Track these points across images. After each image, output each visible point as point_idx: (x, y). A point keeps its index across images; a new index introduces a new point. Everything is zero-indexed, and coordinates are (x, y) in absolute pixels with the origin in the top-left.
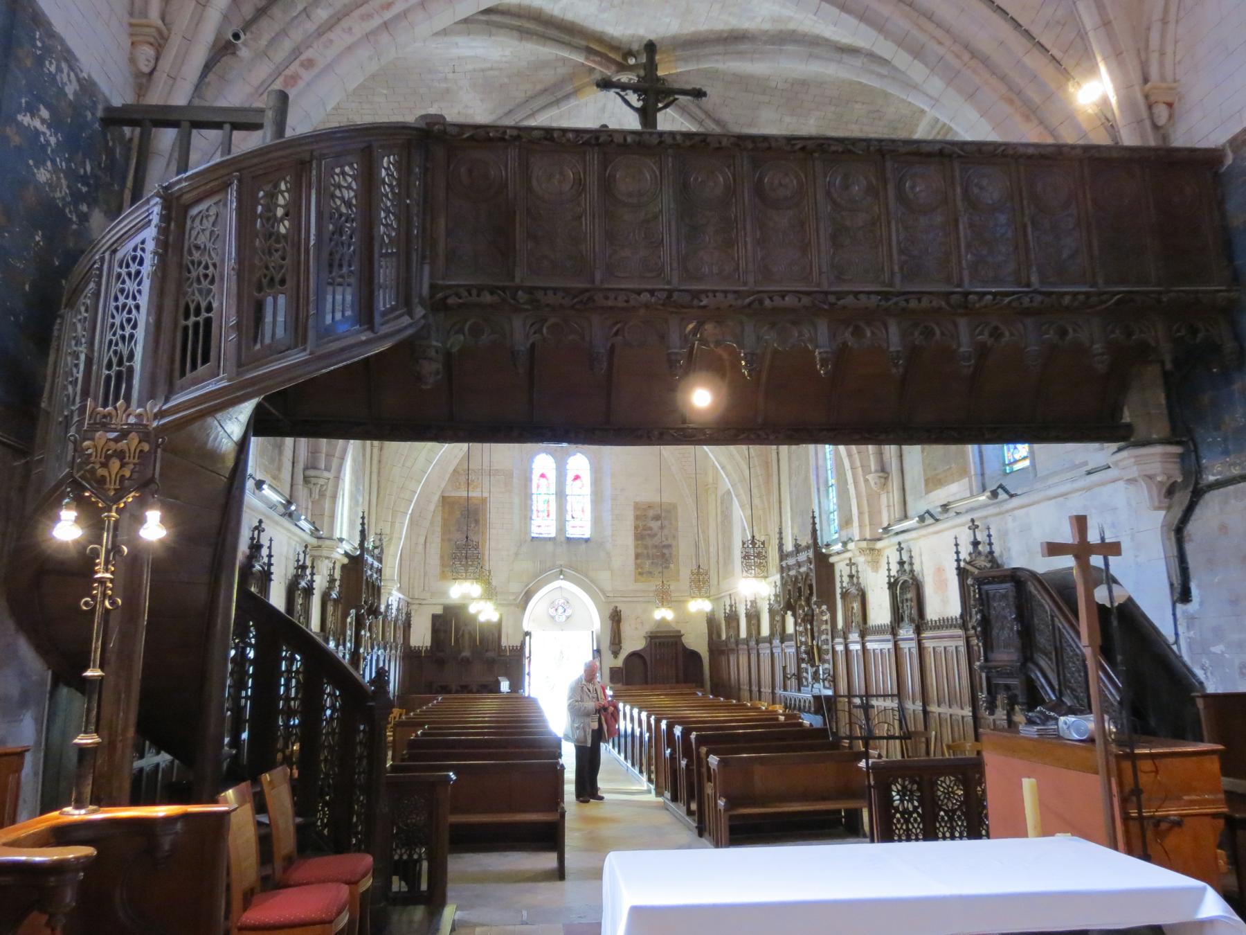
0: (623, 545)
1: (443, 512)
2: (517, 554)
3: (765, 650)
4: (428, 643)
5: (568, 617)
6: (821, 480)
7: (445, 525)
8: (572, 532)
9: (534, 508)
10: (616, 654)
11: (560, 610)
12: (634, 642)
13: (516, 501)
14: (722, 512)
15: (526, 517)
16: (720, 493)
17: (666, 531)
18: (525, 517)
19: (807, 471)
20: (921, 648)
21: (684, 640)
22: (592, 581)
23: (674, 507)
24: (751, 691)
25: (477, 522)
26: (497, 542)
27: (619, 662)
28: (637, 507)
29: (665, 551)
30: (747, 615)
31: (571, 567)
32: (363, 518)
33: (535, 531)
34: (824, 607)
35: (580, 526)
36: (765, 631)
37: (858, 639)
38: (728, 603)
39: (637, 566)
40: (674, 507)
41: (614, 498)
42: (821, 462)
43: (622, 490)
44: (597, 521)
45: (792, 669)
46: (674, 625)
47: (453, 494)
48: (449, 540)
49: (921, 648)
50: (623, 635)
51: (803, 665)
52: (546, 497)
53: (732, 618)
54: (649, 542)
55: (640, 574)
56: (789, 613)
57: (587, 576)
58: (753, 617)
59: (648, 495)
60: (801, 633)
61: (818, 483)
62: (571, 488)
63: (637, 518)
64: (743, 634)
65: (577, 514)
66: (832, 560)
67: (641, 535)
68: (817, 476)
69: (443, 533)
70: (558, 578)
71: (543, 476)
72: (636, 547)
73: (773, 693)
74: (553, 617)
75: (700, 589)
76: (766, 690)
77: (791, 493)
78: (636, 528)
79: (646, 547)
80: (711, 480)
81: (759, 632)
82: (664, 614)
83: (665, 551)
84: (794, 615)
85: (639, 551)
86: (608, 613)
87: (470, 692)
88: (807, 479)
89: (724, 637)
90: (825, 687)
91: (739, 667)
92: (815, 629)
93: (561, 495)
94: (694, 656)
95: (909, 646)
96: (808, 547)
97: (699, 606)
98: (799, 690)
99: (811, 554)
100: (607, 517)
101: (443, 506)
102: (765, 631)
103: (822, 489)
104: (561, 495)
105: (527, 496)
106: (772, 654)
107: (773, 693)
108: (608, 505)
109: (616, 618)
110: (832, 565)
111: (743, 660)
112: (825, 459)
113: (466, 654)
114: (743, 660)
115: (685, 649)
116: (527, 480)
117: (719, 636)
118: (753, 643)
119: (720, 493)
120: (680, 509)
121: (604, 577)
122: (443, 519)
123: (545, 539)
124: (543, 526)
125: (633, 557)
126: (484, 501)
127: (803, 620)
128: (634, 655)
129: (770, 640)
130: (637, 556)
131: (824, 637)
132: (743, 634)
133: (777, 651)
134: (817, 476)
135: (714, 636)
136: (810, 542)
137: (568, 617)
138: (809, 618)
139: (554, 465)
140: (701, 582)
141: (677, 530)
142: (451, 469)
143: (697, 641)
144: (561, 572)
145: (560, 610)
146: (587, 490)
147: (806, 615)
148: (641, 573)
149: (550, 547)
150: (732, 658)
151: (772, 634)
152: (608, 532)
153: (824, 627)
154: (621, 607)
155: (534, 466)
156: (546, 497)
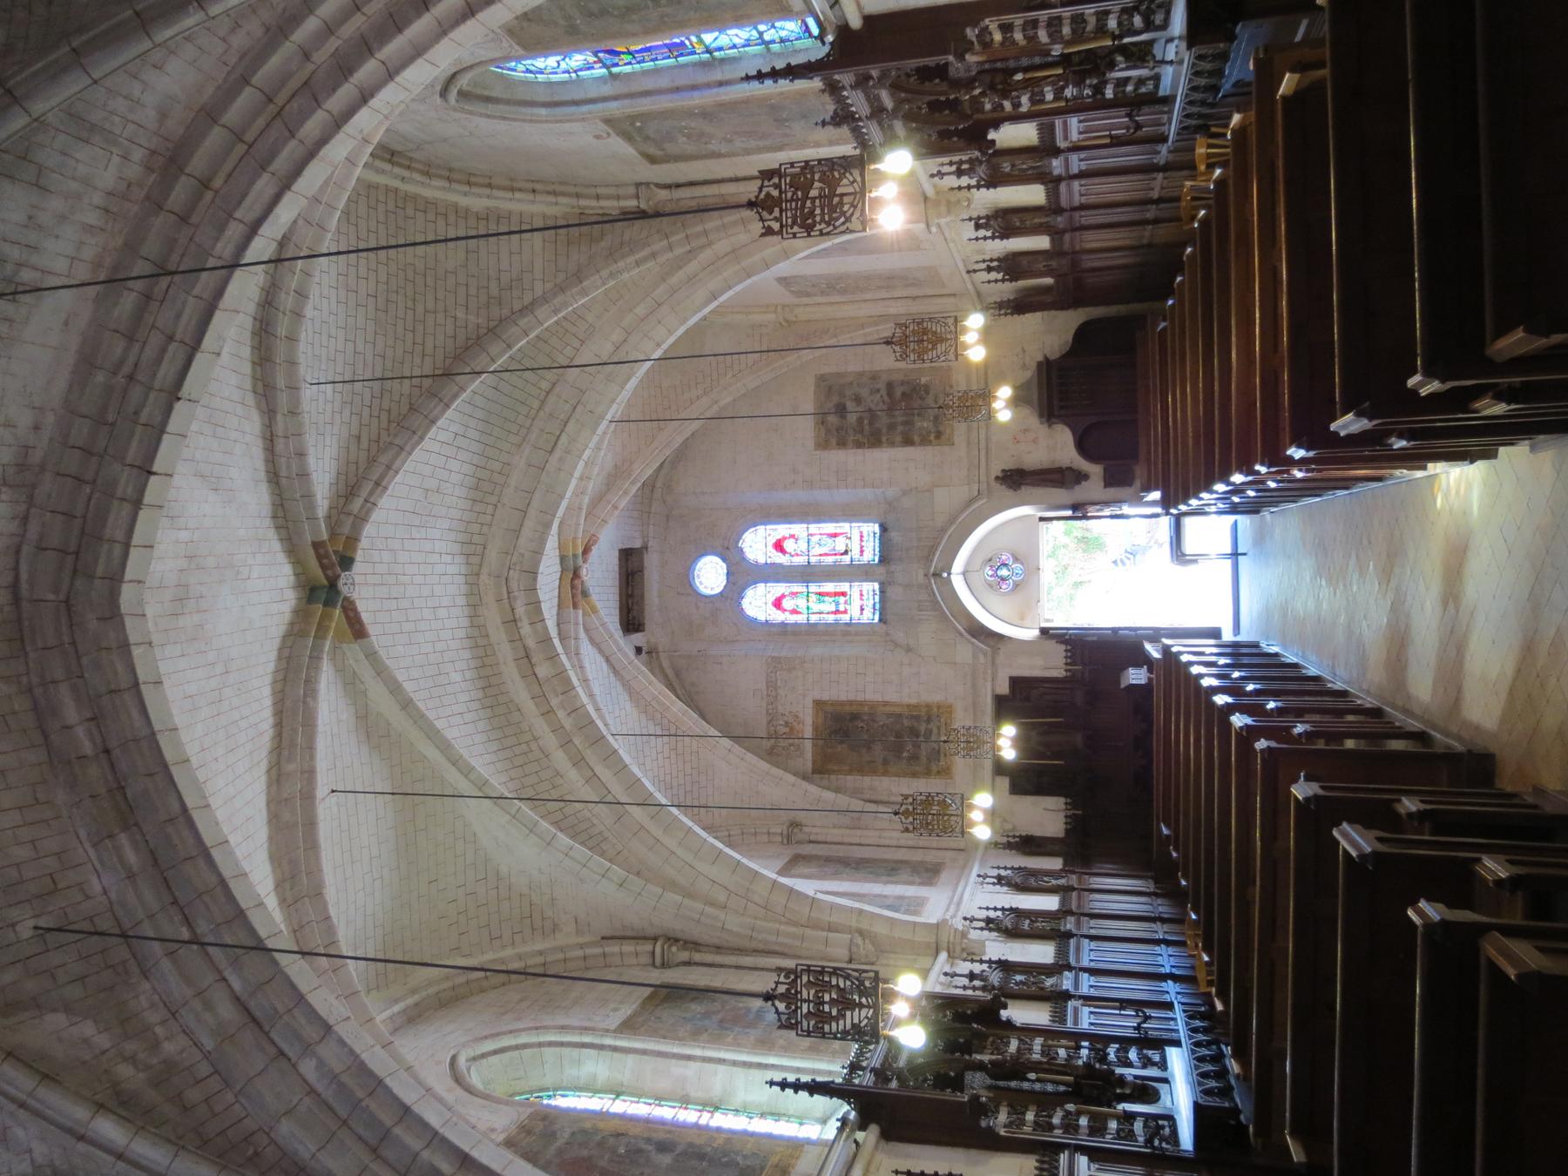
0: (888, 466)
1: (838, 772)
2: (909, 650)
3: (1075, 192)
4: (1062, 800)
5: (1016, 560)
6: (701, 77)
7: (861, 770)
8: (871, 554)
9: (831, 618)
10: (1080, 477)
11: (1004, 572)
12: (1059, 445)
13: (817, 651)
14: (823, 293)
15: (849, 632)
16: (790, 299)
17: (864, 392)
18: (846, 634)
19: (689, 113)
20: (1076, 148)
21: (1054, 354)
22: (952, 521)
23: (821, 379)
24: (1156, 221)
25: (855, 717)
26: (886, 685)
27: (1095, 470)
28: (823, 445)
29: (898, 392)
30: (1004, 235)
31: (928, 559)
32: (784, 1085)
33: (870, 616)
34: (971, 33)
35: (859, 540)
36: (1032, 194)
37: (1062, 158)
38: (984, 276)
39: (925, 441)
40: (821, 379)
41: (810, 484)
42: (664, 82)
43: (795, 471)
44: (850, 513)
45: (1117, 121)
46: (1029, 374)
47: (809, 755)
48: (886, 762)
49: (1076, 148)
50: (1046, 466)
51: (1109, 93)
52: (813, 598)
53: (1012, 266)
54: (883, 420)
55: (939, 435)
56: (991, 135)
57: (944, 530)
58: (1005, 222)
59: (806, 429)
60: (1037, 99)
61: (708, 86)
62: (796, 555)
63: (842, 444)
64: (1042, 242)
65: (840, 544)
66: (855, 22)
67: (871, 436)
68: (694, 88)
69: (874, 772)
70: (948, 582)
71: (778, 604)
72: (892, 444)
73: (1165, 168)
74: (1016, 585)
75: (939, 339)
76: (1157, 185)
77: (748, 152)
78: (859, 445)
79: (892, 427)
80: (771, 317)
81: (1036, 209)
82: (1002, 405)
83: (898, 392)
84: (996, 125)
85: (899, 439)
86: (1004, 492)
87: (1148, 733)
88: (705, 114)
89: (1049, 281)
90: (1165, 26)
91: (1103, 245)
92: (1025, 62)
93: (807, 574)
94: (1083, 334)
95: (1076, 163)
96: (833, 88)
97: (975, 337)
98: (1168, 100)
99: (845, 78)
100: (842, 495)
101: (830, 772)
102: (1032, 194)
103: (718, 75)
104: (807, 574)
105: (812, 632)
106: (1082, 175)
107: (1165, 168)
108: (821, 495)
109: (1017, 480)
110: (869, 20)
111: (1092, 240)
112: (656, 71)
113: (1078, 739)
114: (1092, 240)
115: (1064, 357)
116: (784, 631)
117: (1046, 290)
118: (1060, 221)
119: (790, 299)
120: (826, 370)
121: (946, 499)
122: (850, 772)
123: (882, 600)
124: (861, 603)
125: (910, 450)
126: (818, 704)
127: (1005, 94)
128: (1082, 447)
129: (1052, 182)
130: (908, 442)
131: (1043, 36)
132: (1042, 242)
133: (1076, 163)
134: (694, 88)
135: (1048, 299)
136: (817, 83)
137: (1016, 560)
138: (998, 79)
139: (761, 586)
140: (926, 335)
141: (861, 374)
142: (764, 765)
143: (1049, 333)
144: (937, 575)
145: (1004, 572)
146: (798, 529)
147: (992, 87)
148: (937, 436)
149: (895, 592)
150: (1089, 262)
151: (1042, 177)
152: (868, 494)
153: (1025, 100)
154: (996, 470)
155: (762, 617)
156: (813, 598)
